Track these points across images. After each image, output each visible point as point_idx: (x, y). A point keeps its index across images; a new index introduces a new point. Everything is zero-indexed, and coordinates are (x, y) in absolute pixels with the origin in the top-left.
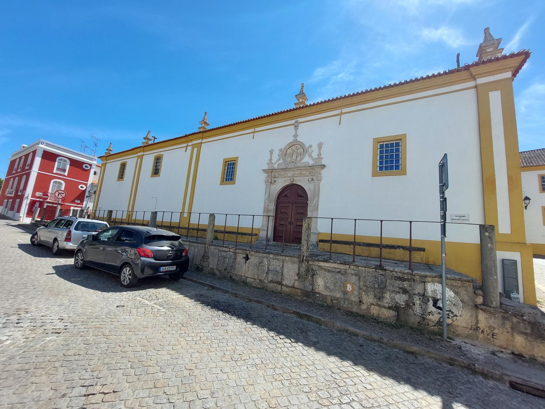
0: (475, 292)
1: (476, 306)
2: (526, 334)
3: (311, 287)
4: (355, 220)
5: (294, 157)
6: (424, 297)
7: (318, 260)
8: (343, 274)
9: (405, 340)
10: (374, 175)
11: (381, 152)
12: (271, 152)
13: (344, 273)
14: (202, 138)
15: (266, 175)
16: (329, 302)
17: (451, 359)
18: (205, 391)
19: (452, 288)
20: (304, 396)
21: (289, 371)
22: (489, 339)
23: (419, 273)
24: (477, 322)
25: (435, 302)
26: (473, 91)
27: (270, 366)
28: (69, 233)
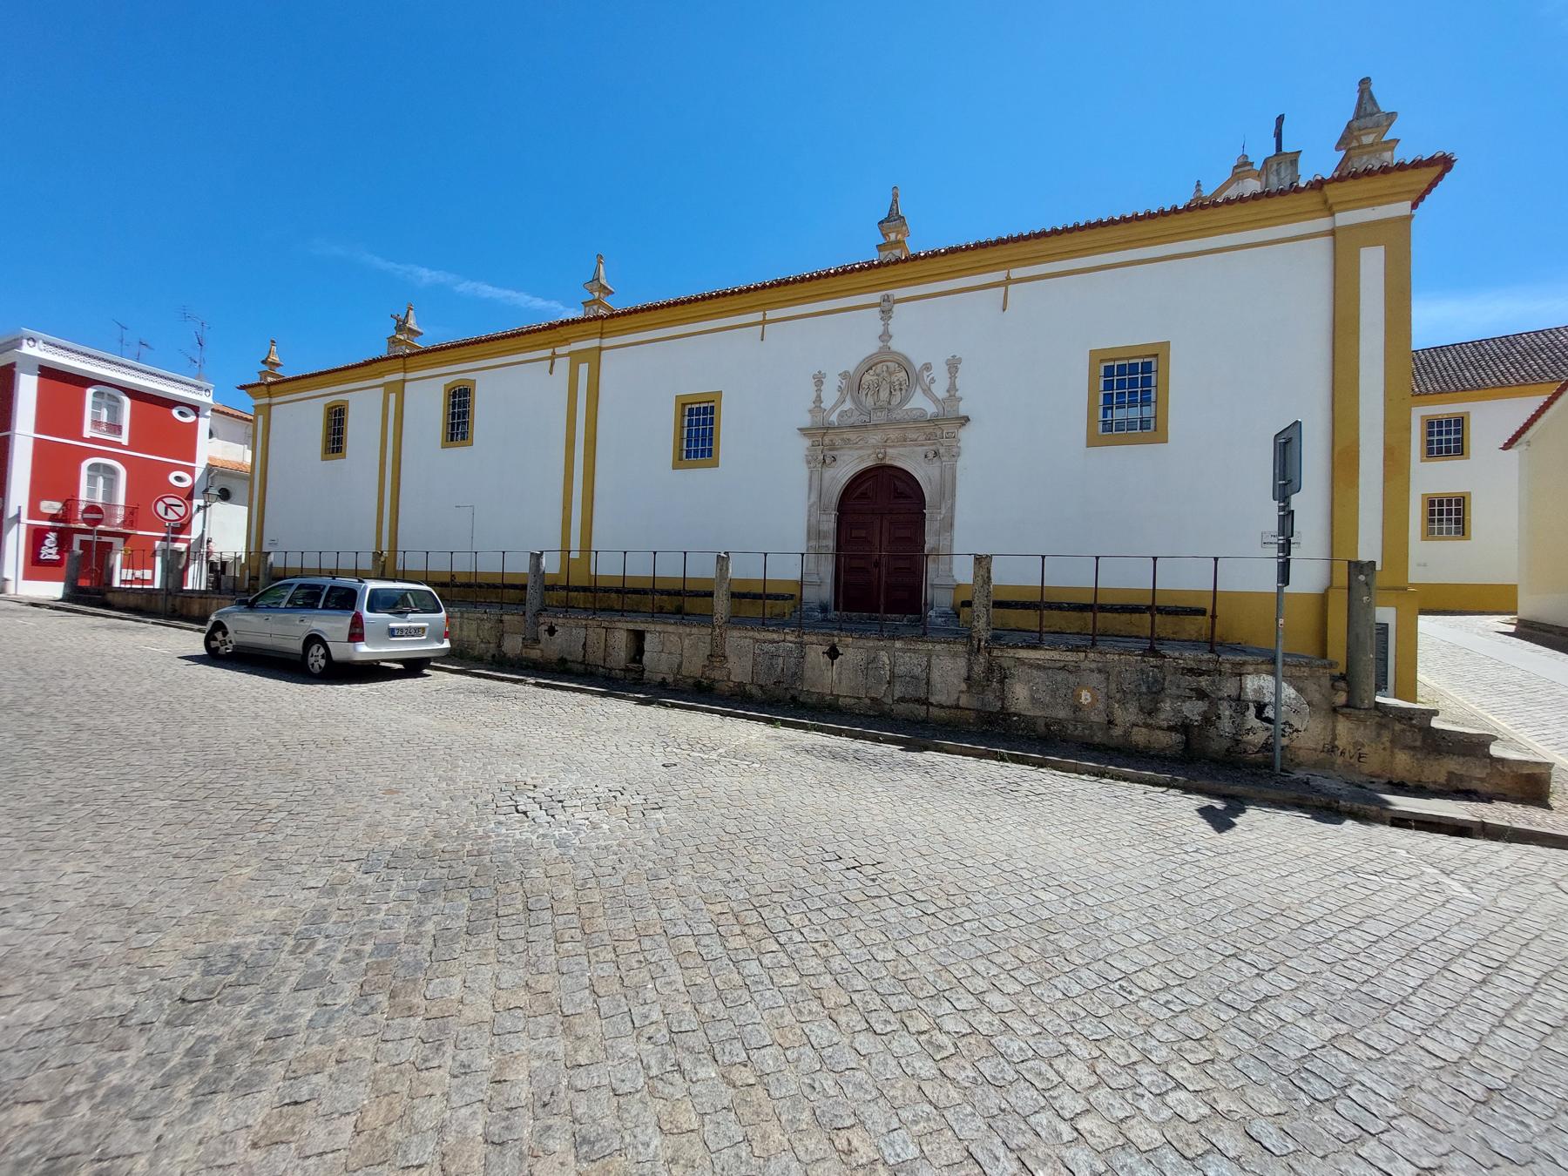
1: (1335, 710)
2: (1414, 748)
3: (999, 704)
5: (884, 395)
6: (1239, 702)
7: (1016, 647)
11: (1108, 385)
12: (819, 380)
13: (1076, 670)
14: (602, 335)
15: (807, 442)
24: (1334, 738)
25: (1260, 708)
26: (1326, 242)
28: (357, 621)
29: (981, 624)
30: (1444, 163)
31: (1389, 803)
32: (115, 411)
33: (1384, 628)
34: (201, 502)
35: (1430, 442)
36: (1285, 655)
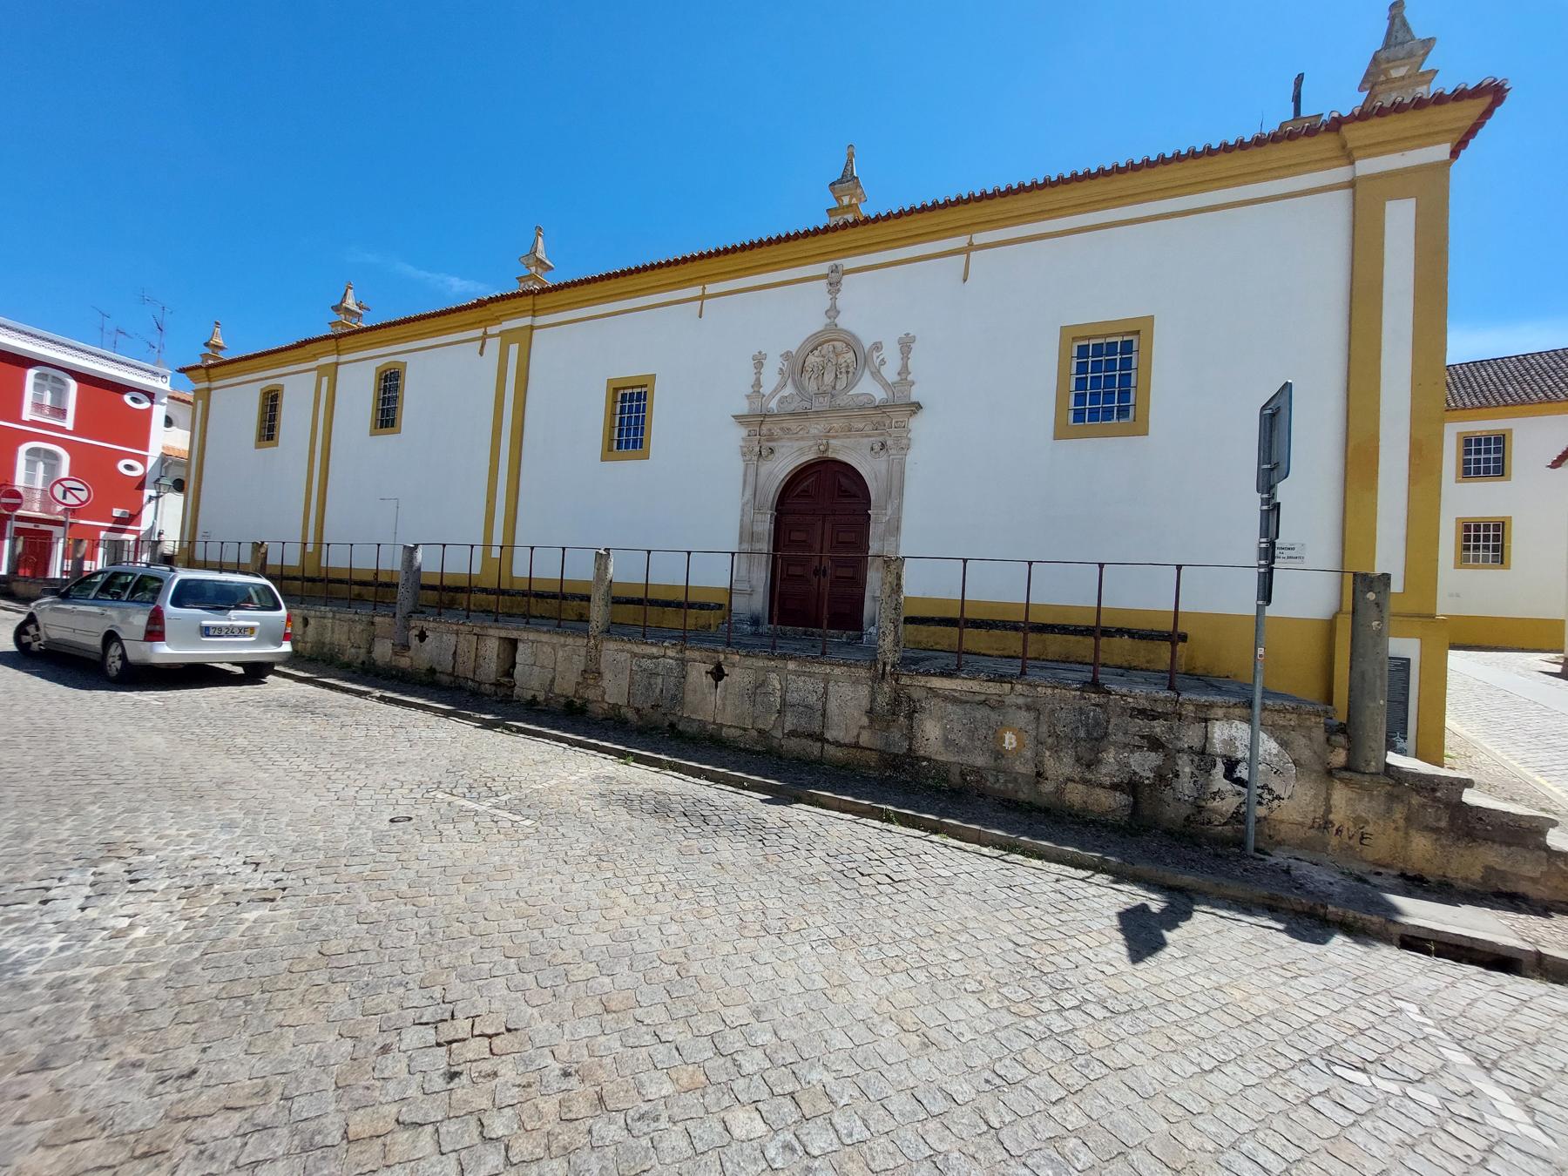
0: (1328, 740)
1: (1330, 773)
2: (1436, 830)
3: (906, 744)
4: (1030, 563)
5: (829, 378)
6: (1203, 755)
7: (927, 674)
8: (993, 708)
9: (1159, 860)
10: (1060, 433)
11: (1082, 368)
12: (759, 362)
13: (997, 705)
14: (535, 313)
15: (743, 432)
16: (955, 779)
17: (1272, 897)
18: (737, 1009)
19: (1274, 731)
20: (971, 1000)
21: (913, 948)
22: (1351, 847)
23: (1194, 697)
24: (1328, 810)
25: (1231, 765)
27: (865, 939)
28: (157, 618)
29: (887, 643)
30: (1494, 93)
31: (1396, 910)
32: (59, 394)
33: (1406, 663)
34: (153, 493)
35: (1467, 462)
36: (1266, 693)
